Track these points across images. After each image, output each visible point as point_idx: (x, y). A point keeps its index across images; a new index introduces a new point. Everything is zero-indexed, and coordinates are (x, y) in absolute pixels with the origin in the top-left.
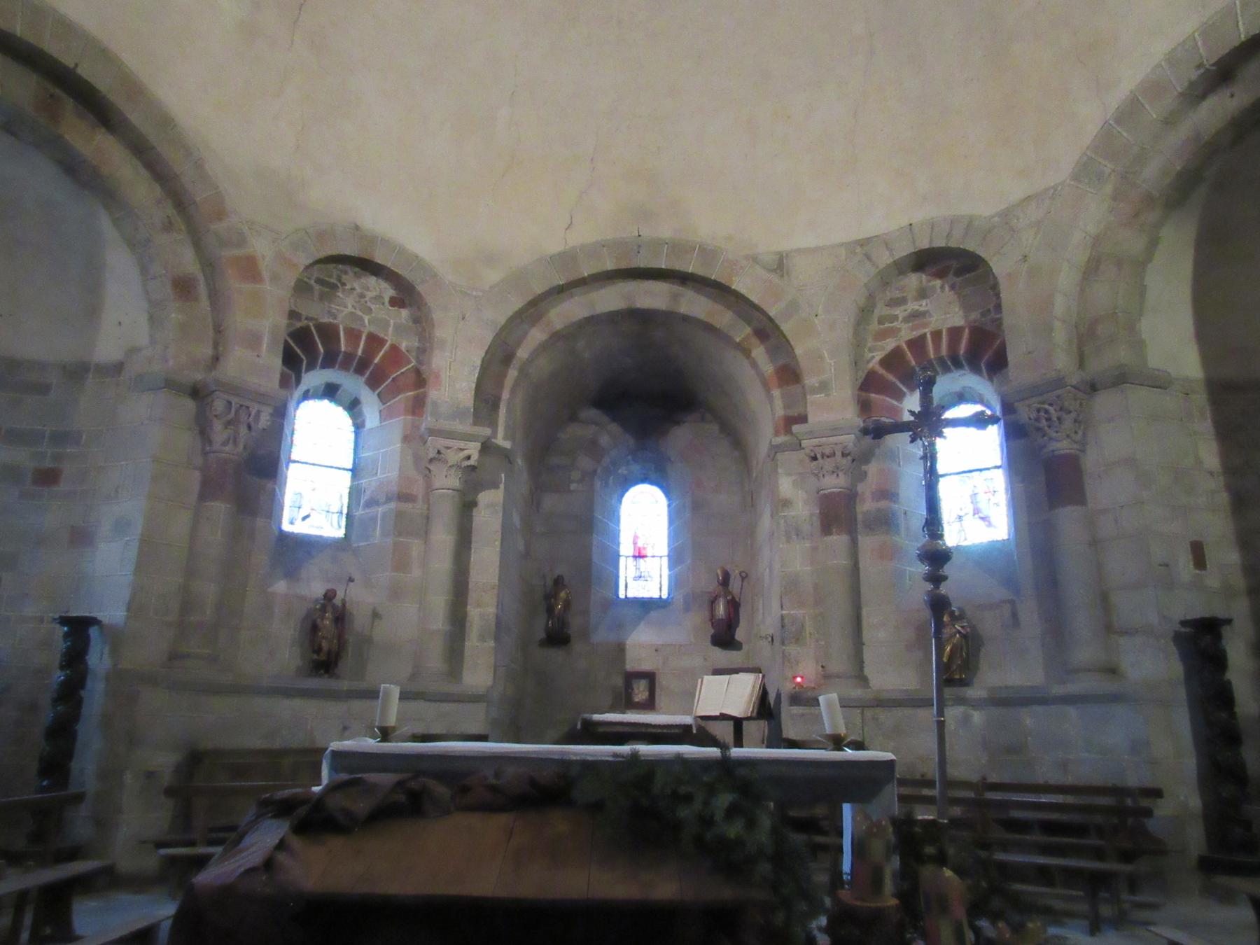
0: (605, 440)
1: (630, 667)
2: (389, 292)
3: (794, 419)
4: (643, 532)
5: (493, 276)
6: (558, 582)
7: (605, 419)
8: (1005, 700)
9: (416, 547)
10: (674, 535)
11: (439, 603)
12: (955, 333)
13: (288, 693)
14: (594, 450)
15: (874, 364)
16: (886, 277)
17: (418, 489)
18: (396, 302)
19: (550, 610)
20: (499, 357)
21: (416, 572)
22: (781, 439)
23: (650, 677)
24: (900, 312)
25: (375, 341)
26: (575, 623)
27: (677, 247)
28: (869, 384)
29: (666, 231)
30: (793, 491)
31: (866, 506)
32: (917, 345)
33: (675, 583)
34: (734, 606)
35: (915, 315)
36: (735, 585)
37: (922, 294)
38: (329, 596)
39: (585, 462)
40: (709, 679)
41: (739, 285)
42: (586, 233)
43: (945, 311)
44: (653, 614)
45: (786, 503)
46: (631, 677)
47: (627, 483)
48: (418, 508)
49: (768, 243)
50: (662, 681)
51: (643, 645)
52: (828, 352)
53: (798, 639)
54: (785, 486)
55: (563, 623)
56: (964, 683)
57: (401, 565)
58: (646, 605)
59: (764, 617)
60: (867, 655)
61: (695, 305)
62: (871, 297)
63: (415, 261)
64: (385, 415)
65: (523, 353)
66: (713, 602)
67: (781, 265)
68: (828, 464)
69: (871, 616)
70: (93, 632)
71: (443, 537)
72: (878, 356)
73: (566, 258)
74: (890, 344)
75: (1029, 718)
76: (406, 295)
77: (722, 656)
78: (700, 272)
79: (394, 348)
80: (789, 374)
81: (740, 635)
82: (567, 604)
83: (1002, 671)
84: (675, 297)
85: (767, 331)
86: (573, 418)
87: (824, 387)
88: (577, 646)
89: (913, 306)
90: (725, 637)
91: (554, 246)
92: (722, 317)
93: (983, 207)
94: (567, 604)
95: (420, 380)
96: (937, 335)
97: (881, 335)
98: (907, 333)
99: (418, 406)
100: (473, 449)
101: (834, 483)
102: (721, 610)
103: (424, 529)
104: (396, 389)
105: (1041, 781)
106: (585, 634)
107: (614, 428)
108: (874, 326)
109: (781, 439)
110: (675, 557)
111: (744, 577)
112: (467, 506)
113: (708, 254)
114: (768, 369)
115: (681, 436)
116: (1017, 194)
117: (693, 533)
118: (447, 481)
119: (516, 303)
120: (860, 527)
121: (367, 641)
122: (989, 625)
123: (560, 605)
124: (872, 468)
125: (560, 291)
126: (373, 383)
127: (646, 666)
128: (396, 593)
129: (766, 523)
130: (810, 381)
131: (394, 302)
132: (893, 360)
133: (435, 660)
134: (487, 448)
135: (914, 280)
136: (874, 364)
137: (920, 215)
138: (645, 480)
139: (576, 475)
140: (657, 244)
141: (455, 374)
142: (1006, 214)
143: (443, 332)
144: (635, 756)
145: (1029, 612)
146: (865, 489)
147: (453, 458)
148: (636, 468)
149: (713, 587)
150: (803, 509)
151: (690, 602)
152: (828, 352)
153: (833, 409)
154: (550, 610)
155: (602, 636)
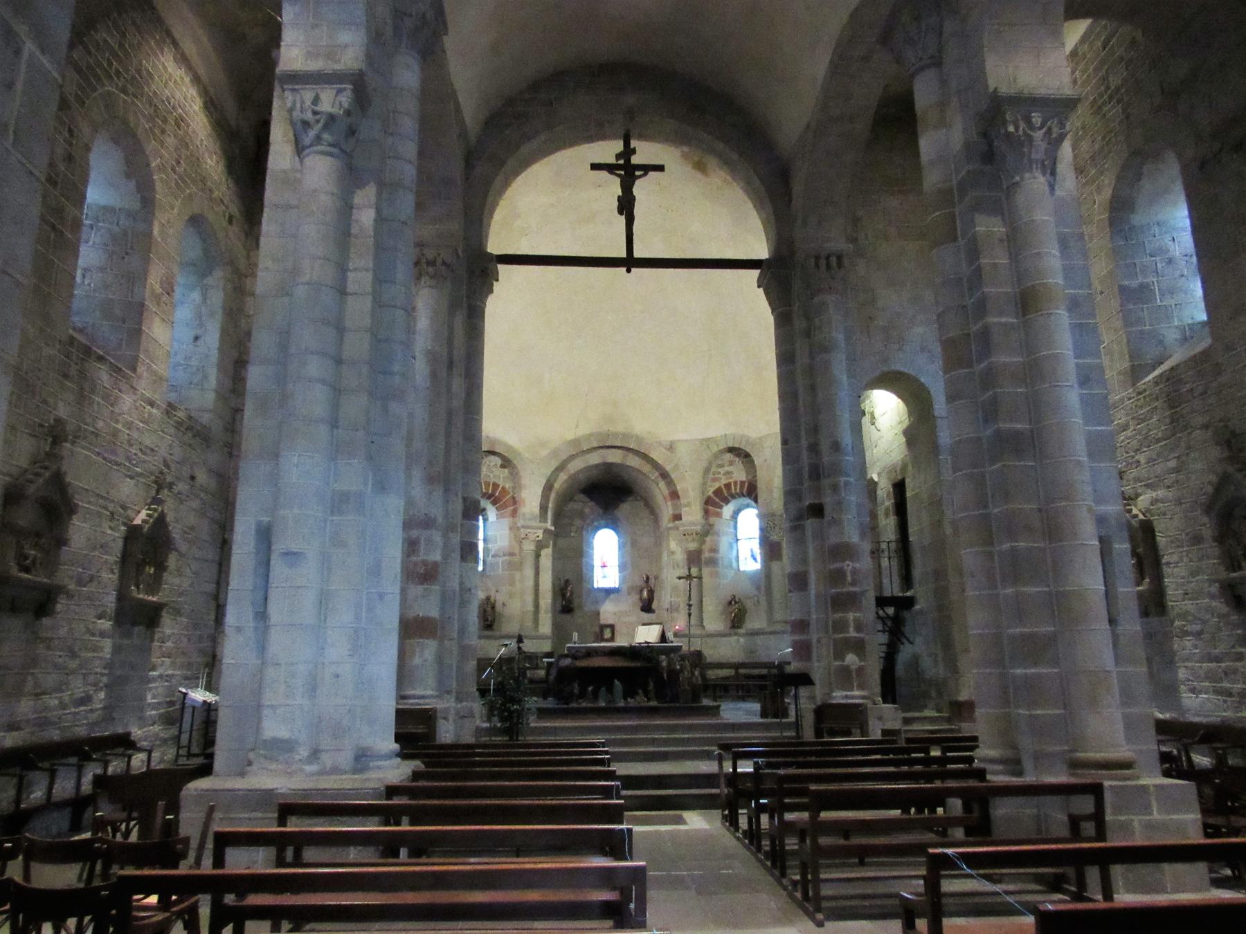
0: (587, 510)
1: (603, 622)
2: (499, 462)
3: (678, 517)
4: (606, 555)
5: (544, 453)
6: (567, 582)
7: (586, 499)
8: (754, 633)
9: (518, 575)
10: (622, 556)
11: (529, 599)
12: (742, 483)
13: (725, 636)
14: (581, 515)
15: (710, 493)
16: (717, 456)
17: (517, 551)
18: (503, 466)
19: (564, 596)
20: (548, 487)
21: (518, 585)
22: (671, 525)
23: (612, 627)
24: (722, 471)
25: (496, 486)
26: (576, 603)
27: (625, 436)
28: (708, 502)
29: (620, 428)
30: (676, 549)
31: (706, 555)
32: (728, 486)
33: (623, 580)
34: (651, 592)
35: (728, 473)
36: (652, 582)
37: (731, 463)
38: (488, 598)
39: (578, 522)
40: (641, 628)
41: (654, 455)
42: (583, 431)
43: (739, 474)
44: (612, 596)
45: (673, 553)
46: (603, 627)
47: (597, 529)
48: (516, 559)
49: (666, 435)
50: (617, 628)
51: (608, 611)
52: (691, 486)
53: (677, 610)
54: (673, 545)
55: (570, 601)
56: (739, 627)
57: (512, 584)
58: (608, 592)
59: (665, 598)
60: (705, 616)
61: (634, 462)
62: (710, 463)
63: (510, 448)
64: (499, 517)
65: (557, 486)
66: (641, 591)
67: (671, 447)
68: (690, 539)
69: (706, 601)
70: (411, 614)
71: (529, 572)
72: (712, 490)
73: (576, 442)
74: (717, 485)
75: (759, 640)
76: (507, 463)
77: (646, 617)
78: (636, 448)
79: (503, 488)
80: (675, 495)
81: (654, 606)
82: (572, 593)
83: (755, 622)
84: (625, 457)
85: (665, 475)
86: (571, 499)
87: (688, 505)
88: (577, 613)
89: (727, 469)
90: (647, 607)
91: (570, 436)
92: (646, 468)
93: (753, 435)
94: (572, 593)
95: (514, 501)
96: (735, 483)
97: (714, 480)
98: (724, 481)
99: (514, 513)
100: (540, 533)
101: (693, 546)
102: (645, 594)
103: (519, 566)
104: (504, 506)
105: (765, 660)
106: (580, 607)
107: (591, 504)
108: (711, 476)
109: (671, 525)
110: (622, 567)
111: (656, 578)
112: (538, 556)
113: (639, 440)
114: (666, 492)
115: (625, 508)
116: (765, 433)
117: (633, 554)
118: (529, 547)
119: (555, 464)
120: (611, 705)
121: (501, 615)
122: (749, 604)
123: (570, 595)
124: (708, 539)
125: (572, 457)
126: (494, 503)
127: (610, 622)
128: (511, 595)
129: (665, 558)
130: (683, 501)
131: (503, 466)
132: (718, 492)
133: (529, 623)
134: (546, 531)
135: (728, 456)
136: (710, 493)
137: (730, 431)
138: (606, 526)
139: (574, 529)
140: (616, 435)
141: (531, 498)
142: (760, 438)
143: (525, 481)
144: (137, 869)
145: (763, 599)
146: (706, 547)
147: (532, 537)
148: (603, 522)
149: (641, 583)
150: (680, 556)
151: (631, 590)
152: (691, 486)
153: (693, 514)
154: (564, 596)
155: (588, 607)
